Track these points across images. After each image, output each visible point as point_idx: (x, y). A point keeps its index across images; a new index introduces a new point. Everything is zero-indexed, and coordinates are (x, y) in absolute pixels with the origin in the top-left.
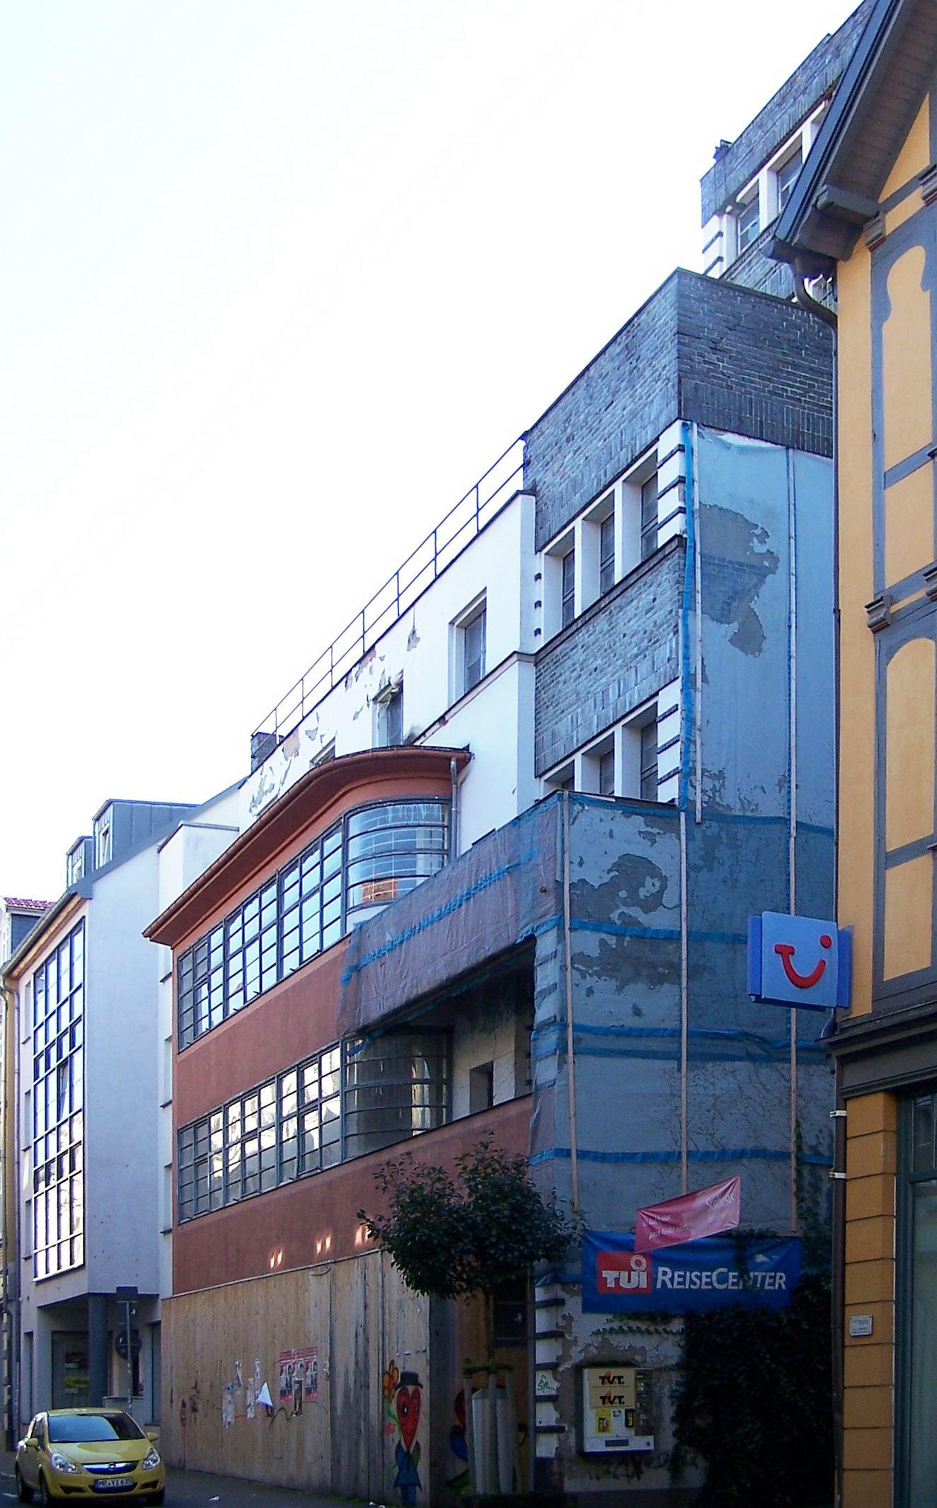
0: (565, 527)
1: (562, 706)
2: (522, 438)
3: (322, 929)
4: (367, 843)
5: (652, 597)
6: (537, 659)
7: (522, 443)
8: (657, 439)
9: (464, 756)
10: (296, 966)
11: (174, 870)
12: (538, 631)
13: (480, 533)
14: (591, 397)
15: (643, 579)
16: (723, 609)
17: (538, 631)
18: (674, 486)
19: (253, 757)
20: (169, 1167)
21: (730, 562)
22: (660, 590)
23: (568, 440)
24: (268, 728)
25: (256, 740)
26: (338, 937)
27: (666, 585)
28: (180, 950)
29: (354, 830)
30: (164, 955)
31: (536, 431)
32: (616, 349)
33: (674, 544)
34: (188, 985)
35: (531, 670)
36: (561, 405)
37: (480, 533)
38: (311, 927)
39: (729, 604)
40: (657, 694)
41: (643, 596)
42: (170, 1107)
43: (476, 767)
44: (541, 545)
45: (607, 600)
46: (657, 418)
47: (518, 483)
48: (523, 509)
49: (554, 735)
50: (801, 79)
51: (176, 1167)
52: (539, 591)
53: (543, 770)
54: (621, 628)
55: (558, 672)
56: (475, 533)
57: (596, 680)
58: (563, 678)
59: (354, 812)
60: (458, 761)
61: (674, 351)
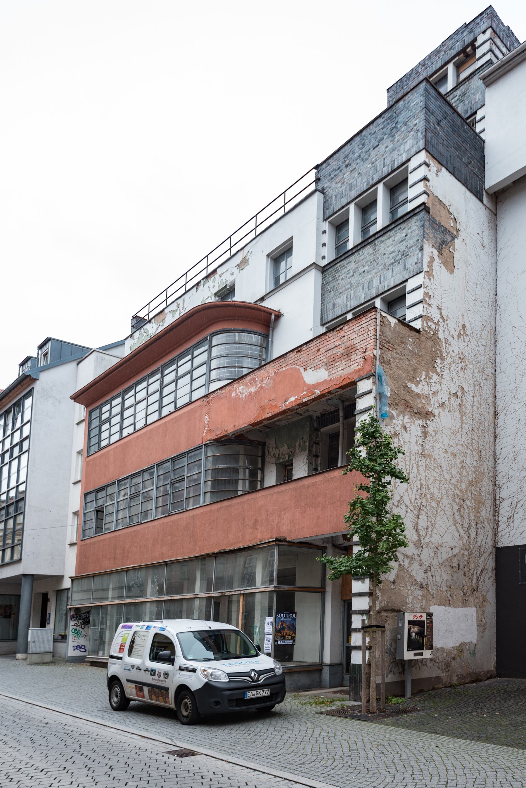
0: (343, 207)
1: (340, 290)
2: (317, 167)
3: (147, 416)
4: (228, 349)
5: (404, 235)
6: (324, 270)
7: (314, 171)
8: (409, 160)
9: (279, 316)
10: (97, 450)
11: (88, 372)
12: (324, 257)
13: (187, 292)
14: (363, 145)
15: (399, 227)
16: (439, 247)
17: (324, 257)
18: (421, 181)
19: (132, 326)
20: (75, 513)
21: (442, 226)
22: (410, 231)
23: (347, 166)
24: (141, 315)
25: (135, 320)
26: (118, 439)
27: (415, 227)
28: (91, 408)
29: (214, 342)
30: (80, 411)
31: (325, 165)
32: (381, 120)
33: (421, 208)
34: (95, 423)
35: (319, 275)
36: (343, 150)
37: (187, 292)
38: (141, 415)
39: (442, 245)
40: (406, 281)
41: (398, 234)
42: (79, 485)
43: (283, 321)
44: (327, 216)
45: (393, 226)
46: (410, 149)
47: (312, 187)
48: (317, 199)
49: (334, 305)
50: (404, 79)
51: (81, 515)
52: (326, 238)
53: (326, 321)
54: (382, 251)
55: (337, 275)
56: (184, 291)
57: (364, 277)
58: (341, 277)
59: (216, 333)
60: (275, 315)
61: (423, 117)
